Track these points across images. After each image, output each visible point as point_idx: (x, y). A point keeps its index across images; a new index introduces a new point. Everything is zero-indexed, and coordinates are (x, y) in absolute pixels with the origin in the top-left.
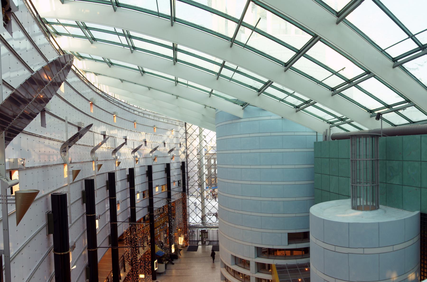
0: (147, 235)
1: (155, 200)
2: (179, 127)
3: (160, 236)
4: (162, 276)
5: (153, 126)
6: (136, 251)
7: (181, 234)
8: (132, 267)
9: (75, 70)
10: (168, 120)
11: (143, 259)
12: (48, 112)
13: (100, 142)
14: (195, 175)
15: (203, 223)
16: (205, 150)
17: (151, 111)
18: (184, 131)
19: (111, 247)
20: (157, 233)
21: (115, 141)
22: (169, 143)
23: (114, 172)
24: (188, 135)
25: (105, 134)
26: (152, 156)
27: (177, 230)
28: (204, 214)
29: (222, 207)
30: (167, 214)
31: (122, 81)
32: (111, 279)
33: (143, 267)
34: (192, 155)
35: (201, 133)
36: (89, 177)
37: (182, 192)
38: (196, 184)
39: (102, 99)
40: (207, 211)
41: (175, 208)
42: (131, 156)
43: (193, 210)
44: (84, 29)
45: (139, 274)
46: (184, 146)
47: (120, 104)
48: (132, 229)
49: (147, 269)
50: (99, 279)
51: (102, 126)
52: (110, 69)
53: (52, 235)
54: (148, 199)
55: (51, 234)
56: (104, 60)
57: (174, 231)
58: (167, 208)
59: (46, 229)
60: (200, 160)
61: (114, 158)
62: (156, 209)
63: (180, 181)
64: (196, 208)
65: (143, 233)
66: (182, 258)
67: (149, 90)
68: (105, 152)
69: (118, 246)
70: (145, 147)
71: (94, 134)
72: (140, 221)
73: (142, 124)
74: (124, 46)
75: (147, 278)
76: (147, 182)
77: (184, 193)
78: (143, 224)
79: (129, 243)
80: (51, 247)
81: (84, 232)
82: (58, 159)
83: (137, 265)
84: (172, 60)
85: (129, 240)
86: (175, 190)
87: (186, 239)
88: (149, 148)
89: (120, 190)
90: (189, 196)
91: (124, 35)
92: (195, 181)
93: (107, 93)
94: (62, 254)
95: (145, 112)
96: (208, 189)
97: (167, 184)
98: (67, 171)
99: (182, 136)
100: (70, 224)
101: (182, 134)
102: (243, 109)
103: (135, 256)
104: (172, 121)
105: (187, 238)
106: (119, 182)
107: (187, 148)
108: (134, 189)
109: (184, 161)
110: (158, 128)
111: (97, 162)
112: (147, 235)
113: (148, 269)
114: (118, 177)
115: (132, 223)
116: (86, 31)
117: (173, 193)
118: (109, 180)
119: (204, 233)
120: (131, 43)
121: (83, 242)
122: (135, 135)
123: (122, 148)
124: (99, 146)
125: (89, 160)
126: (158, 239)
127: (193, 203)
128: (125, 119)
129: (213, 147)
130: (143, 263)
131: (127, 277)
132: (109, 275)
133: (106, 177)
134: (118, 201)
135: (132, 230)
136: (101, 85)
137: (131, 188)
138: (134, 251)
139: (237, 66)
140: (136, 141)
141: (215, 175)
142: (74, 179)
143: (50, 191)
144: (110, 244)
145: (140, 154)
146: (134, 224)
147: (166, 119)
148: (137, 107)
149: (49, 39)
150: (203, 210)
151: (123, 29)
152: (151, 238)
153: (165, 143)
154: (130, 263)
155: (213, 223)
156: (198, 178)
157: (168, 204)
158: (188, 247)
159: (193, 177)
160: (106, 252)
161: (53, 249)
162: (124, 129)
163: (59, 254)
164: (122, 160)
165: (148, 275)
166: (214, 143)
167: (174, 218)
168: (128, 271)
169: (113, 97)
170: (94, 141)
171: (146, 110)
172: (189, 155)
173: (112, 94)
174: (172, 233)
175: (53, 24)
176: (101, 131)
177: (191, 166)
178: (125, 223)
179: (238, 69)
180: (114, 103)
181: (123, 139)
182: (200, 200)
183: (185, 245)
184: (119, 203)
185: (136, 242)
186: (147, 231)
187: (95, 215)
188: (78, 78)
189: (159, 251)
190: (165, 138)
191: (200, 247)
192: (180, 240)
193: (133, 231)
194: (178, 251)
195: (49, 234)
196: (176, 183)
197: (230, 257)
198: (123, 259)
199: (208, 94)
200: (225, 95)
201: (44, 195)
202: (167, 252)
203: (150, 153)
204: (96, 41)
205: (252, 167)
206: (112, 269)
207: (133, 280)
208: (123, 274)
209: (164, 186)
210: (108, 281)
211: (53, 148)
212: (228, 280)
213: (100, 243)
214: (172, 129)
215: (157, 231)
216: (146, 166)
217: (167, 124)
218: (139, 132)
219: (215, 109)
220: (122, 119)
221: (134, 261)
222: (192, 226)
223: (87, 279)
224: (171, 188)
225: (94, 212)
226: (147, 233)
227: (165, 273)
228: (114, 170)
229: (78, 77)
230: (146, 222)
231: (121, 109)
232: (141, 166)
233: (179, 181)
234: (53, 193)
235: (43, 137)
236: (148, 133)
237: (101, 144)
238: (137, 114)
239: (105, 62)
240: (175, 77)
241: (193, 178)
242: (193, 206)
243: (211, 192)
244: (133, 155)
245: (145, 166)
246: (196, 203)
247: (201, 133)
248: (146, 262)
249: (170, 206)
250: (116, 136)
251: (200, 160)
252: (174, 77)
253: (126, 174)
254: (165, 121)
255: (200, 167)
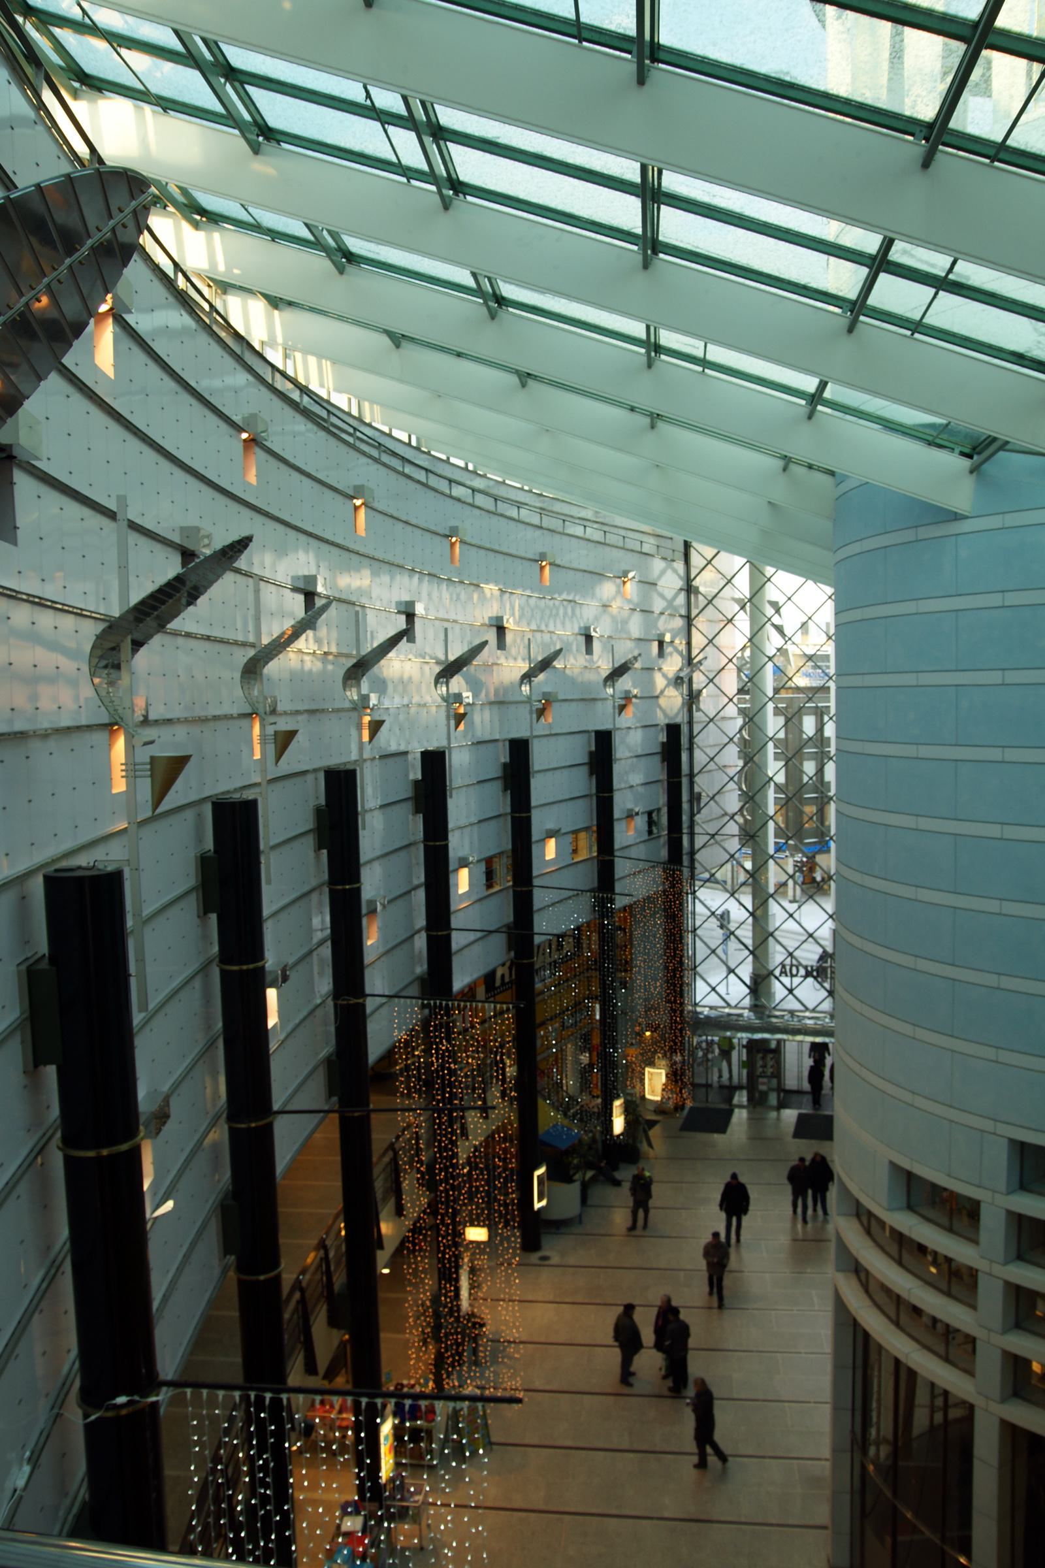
0: (502, 1054)
1: (540, 898)
2: (658, 565)
3: (559, 1059)
4: (565, 1234)
5: (537, 558)
6: (452, 1128)
7: (656, 1052)
8: (433, 1195)
9: (171, 273)
10: (606, 528)
11: (482, 1163)
12: (29, 468)
13: (288, 624)
14: (724, 790)
15: (756, 1008)
16: (778, 670)
17: (526, 488)
18: (679, 583)
19: (336, 1107)
20: (551, 1047)
21: (357, 621)
22: (610, 637)
23: (351, 767)
24: (697, 598)
25: (310, 589)
26: (529, 698)
27: (640, 1034)
28: (767, 970)
29: (856, 941)
30: (596, 960)
31: (398, 339)
32: (338, 1248)
33: (482, 1198)
34: (717, 696)
35: (757, 590)
36: (236, 790)
37: (664, 863)
38: (733, 828)
39: (302, 425)
40: (777, 956)
41: (631, 935)
42: (433, 696)
43: (714, 948)
44: (218, 75)
45: (465, 1226)
46: (676, 650)
47: (385, 452)
48: (436, 1030)
49: (500, 1205)
50: (283, 1250)
51: (297, 551)
52: (340, 282)
53: (51, 1072)
54: (511, 891)
55: (46, 1064)
56: (312, 238)
57: (627, 1042)
58: (595, 937)
59: (22, 1042)
60: (752, 719)
61: (352, 702)
62: (543, 938)
63: (654, 815)
64: (726, 939)
65: (484, 1046)
66: (656, 1158)
67: (524, 385)
68: (310, 671)
69: (371, 1106)
70: (499, 651)
71: (259, 584)
72: (469, 993)
73: (488, 546)
74: (409, 174)
75: (501, 1243)
76: (506, 814)
77: (674, 871)
78: (483, 1007)
79: (419, 1092)
80: (50, 1127)
81: (211, 1045)
82: (82, 704)
83: (453, 1188)
84: (635, 248)
85: (419, 1079)
86: (634, 853)
87: (675, 1077)
88: (515, 659)
89: (378, 853)
90: (698, 883)
91: (410, 125)
92: (726, 814)
93: (325, 397)
94: (105, 1152)
95: (502, 492)
96: (784, 851)
97: (598, 826)
98: (123, 761)
99: (670, 603)
100: (140, 1011)
101: (669, 594)
102: (971, 472)
103: (446, 1149)
104: (623, 532)
105: (682, 1074)
106: (377, 813)
107: (689, 661)
108: (446, 846)
109: (678, 720)
110: (559, 566)
111: (272, 719)
112: (501, 1058)
113: (506, 1205)
114: (369, 790)
115: (435, 1003)
116: (228, 87)
117: (622, 867)
118: (327, 805)
119: (760, 1055)
120: (440, 161)
121: (209, 1091)
122: (455, 598)
123: (390, 655)
124: (280, 645)
125: (235, 711)
126: (550, 1076)
127: (713, 913)
128: (406, 522)
129: (814, 658)
130: (482, 1180)
131: (408, 1237)
132: (327, 1233)
133: (315, 792)
134: (372, 902)
135: (431, 1031)
136: (298, 355)
137: (432, 843)
138: (440, 1125)
139: (952, 259)
140: (457, 628)
141: (819, 786)
142: (157, 802)
143: (46, 852)
144: (330, 1097)
145: (475, 686)
146: (441, 1004)
147: (595, 526)
148: (467, 464)
149: (38, 96)
150: (758, 951)
151: (406, 92)
152: (520, 1070)
153: (589, 639)
154: (423, 1178)
155: (807, 1009)
156: (740, 801)
157: (602, 917)
158: (686, 1112)
159: (717, 798)
160: (313, 1132)
161: (59, 1134)
162: (402, 567)
163: (91, 1154)
164: (391, 711)
165: (502, 1229)
166: (819, 641)
167: (626, 982)
168: (414, 1211)
169: (354, 417)
170: (258, 620)
171: (504, 483)
172: (700, 692)
173: (350, 400)
174: (618, 1048)
175: (57, 22)
176: (294, 574)
177: (711, 746)
178: (402, 1000)
179: (958, 275)
180: (358, 444)
181: (399, 612)
182: (748, 901)
183: (671, 1103)
184: (374, 911)
185: (451, 1085)
186: (502, 1036)
187: (263, 968)
188: (183, 312)
189: (554, 1126)
190: (589, 611)
191: (740, 1116)
192: (650, 1080)
193: (436, 1037)
194: (641, 1128)
195: (36, 1066)
196: (640, 822)
197: (883, 1174)
198: (391, 1160)
199: (803, 402)
200: (887, 403)
201: (11, 881)
202: (591, 1131)
203: (521, 682)
204: (274, 144)
205: (1012, 755)
206: (340, 1205)
207: (439, 1251)
208: (391, 1225)
209: (582, 835)
210: (323, 1256)
211: (53, 646)
212: (867, 1272)
213: (284, 1098)
214: (625, 574)
215: (546, 1037)
216: (500, 744)
217: (600, 547)
218: (470, 584)
219: (832, 473)
220: (395, 521)
221: (441, 1170)
222: (707, 1017)
223: (225, 1256)
224: (616, 846)
225: (256, 950)
226: (502, 1046)
227: (580, 1222)
228: (354, 756)
229: (184, 306)
230: (498, 998)
231: (390, 472)
232: (479, 743)
233: (650, 814)
234: (56, 871)
235: (8, 592)
236: (514, 587)
237: (290, 632)
238: (463, 499)
239: (317, 244)
240: (648, 327)
241: (716, 802)
242: (713, 930)
243: (799, 867)
244: (444, 689)
245: (496, 741)
246: (726, 917)
247: (757, 590)
248: (494, 1175)
249: (608, 924)
250: (364, 601)
251: (752, 719)
252: (644, 326)
253: (407, 775)
254: (593, 533)
255: (751, 752)
